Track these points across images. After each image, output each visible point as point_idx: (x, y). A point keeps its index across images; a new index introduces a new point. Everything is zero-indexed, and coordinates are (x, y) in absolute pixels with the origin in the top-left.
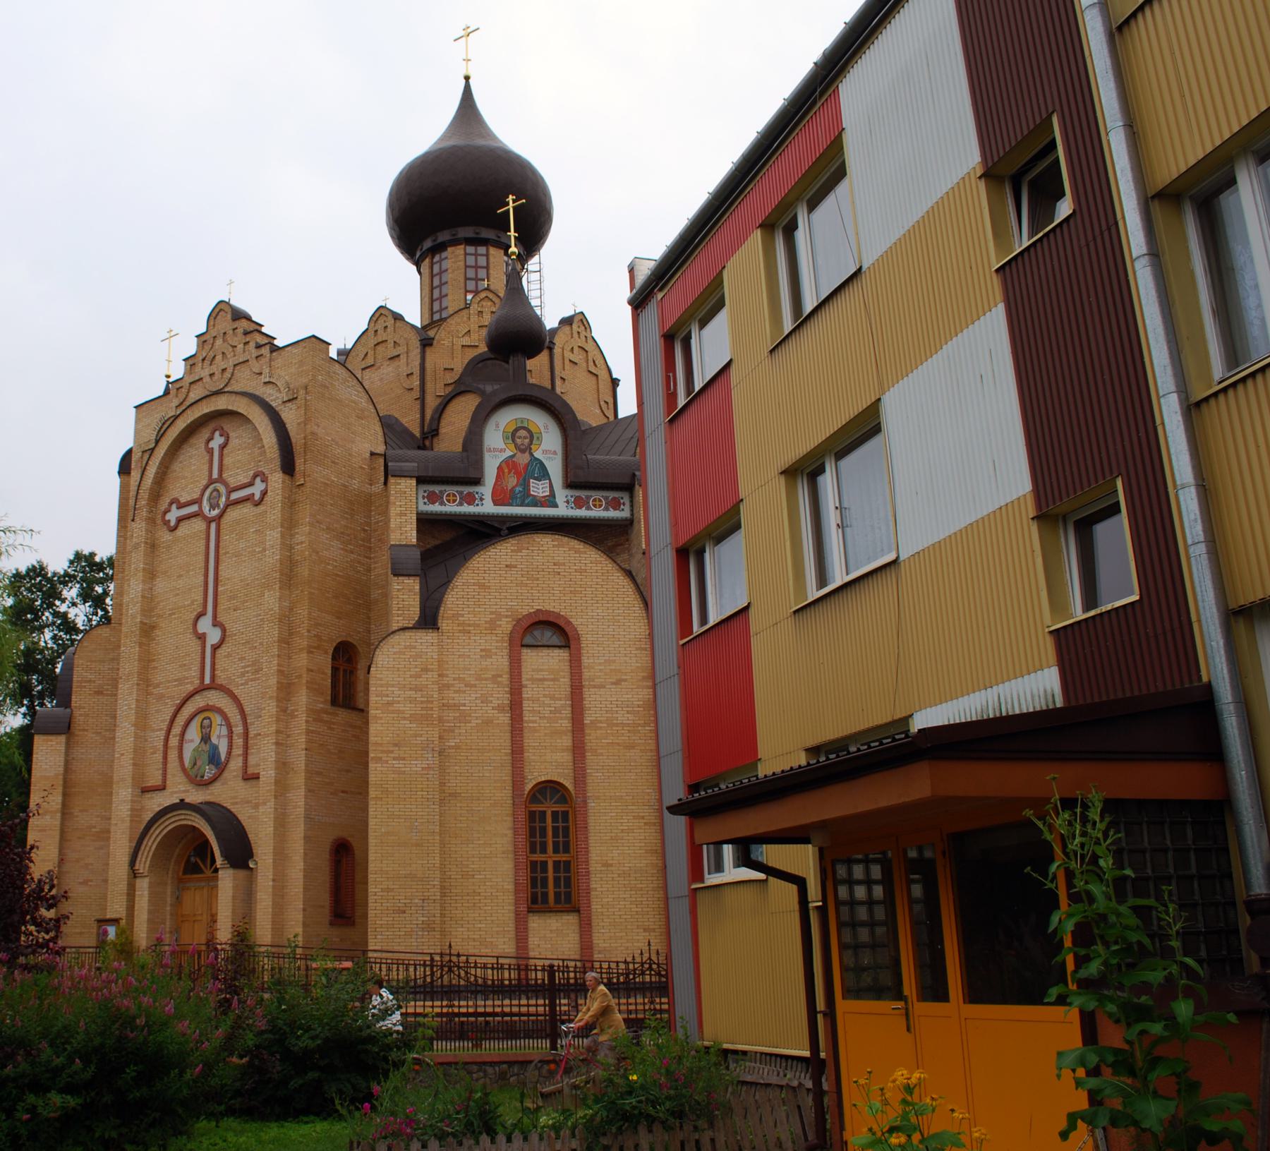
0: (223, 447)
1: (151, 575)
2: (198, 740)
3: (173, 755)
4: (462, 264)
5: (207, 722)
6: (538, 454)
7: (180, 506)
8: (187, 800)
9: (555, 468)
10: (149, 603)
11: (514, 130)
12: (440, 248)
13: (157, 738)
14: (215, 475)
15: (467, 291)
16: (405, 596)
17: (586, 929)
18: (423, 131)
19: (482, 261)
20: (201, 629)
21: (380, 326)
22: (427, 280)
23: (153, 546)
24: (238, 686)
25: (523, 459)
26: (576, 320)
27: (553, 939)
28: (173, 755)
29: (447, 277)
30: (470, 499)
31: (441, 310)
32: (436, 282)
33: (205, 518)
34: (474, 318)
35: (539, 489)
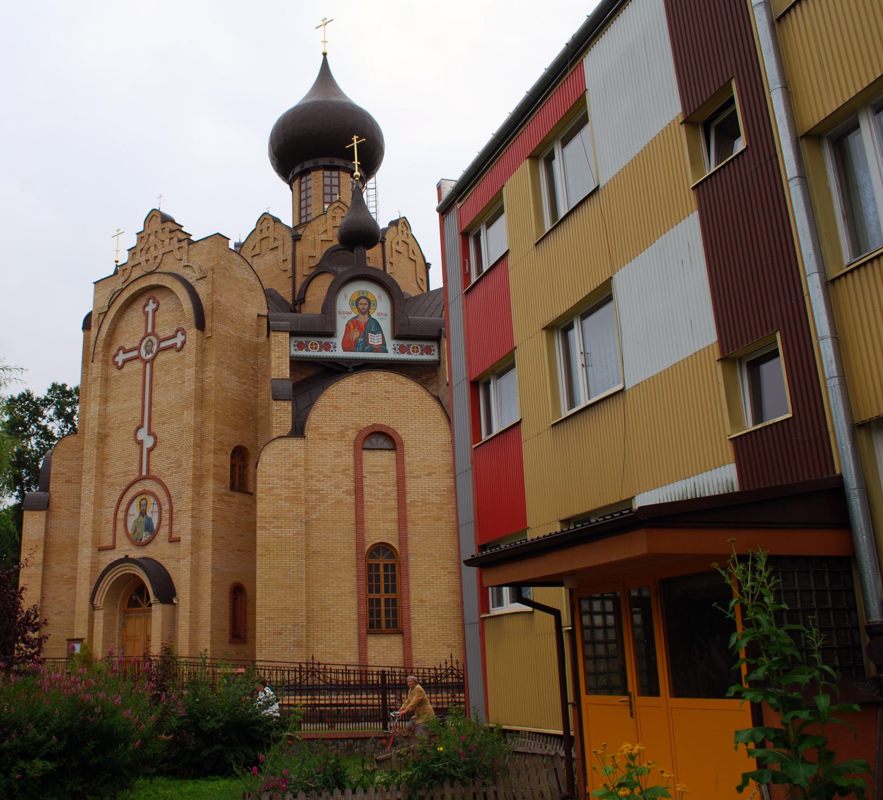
0: (155, 311)
1: (105, 399)
2: (137, 514)
3: (120, 525)
4: (321, 183)
5: (144, 502)
6: (374, 316)
7: (125, 352)
8: (130, 556)
9: (386, 325)
10: (104, 419)
11: (357, 90)
12: (306, 172)
13: (109, 513)
14: (150, 330)
15: (325, 203)
16: (282, 414)
17: (407, 646)
18: (294, 91)
19: (335, 181)
20: (140, 437)
21: (264, 227)
22: (297, 195)
23: (106, 380)
24: (165, 477)
25: (364, 319)
26: (400, 222)
27: (385, 653)
28: (120, 525)
29: (311, 192)
30: (327, 347)
31: (307, 215)
32: (303, 196)
33: (142, 360)
34: (330, 221)
35: (375, 340)
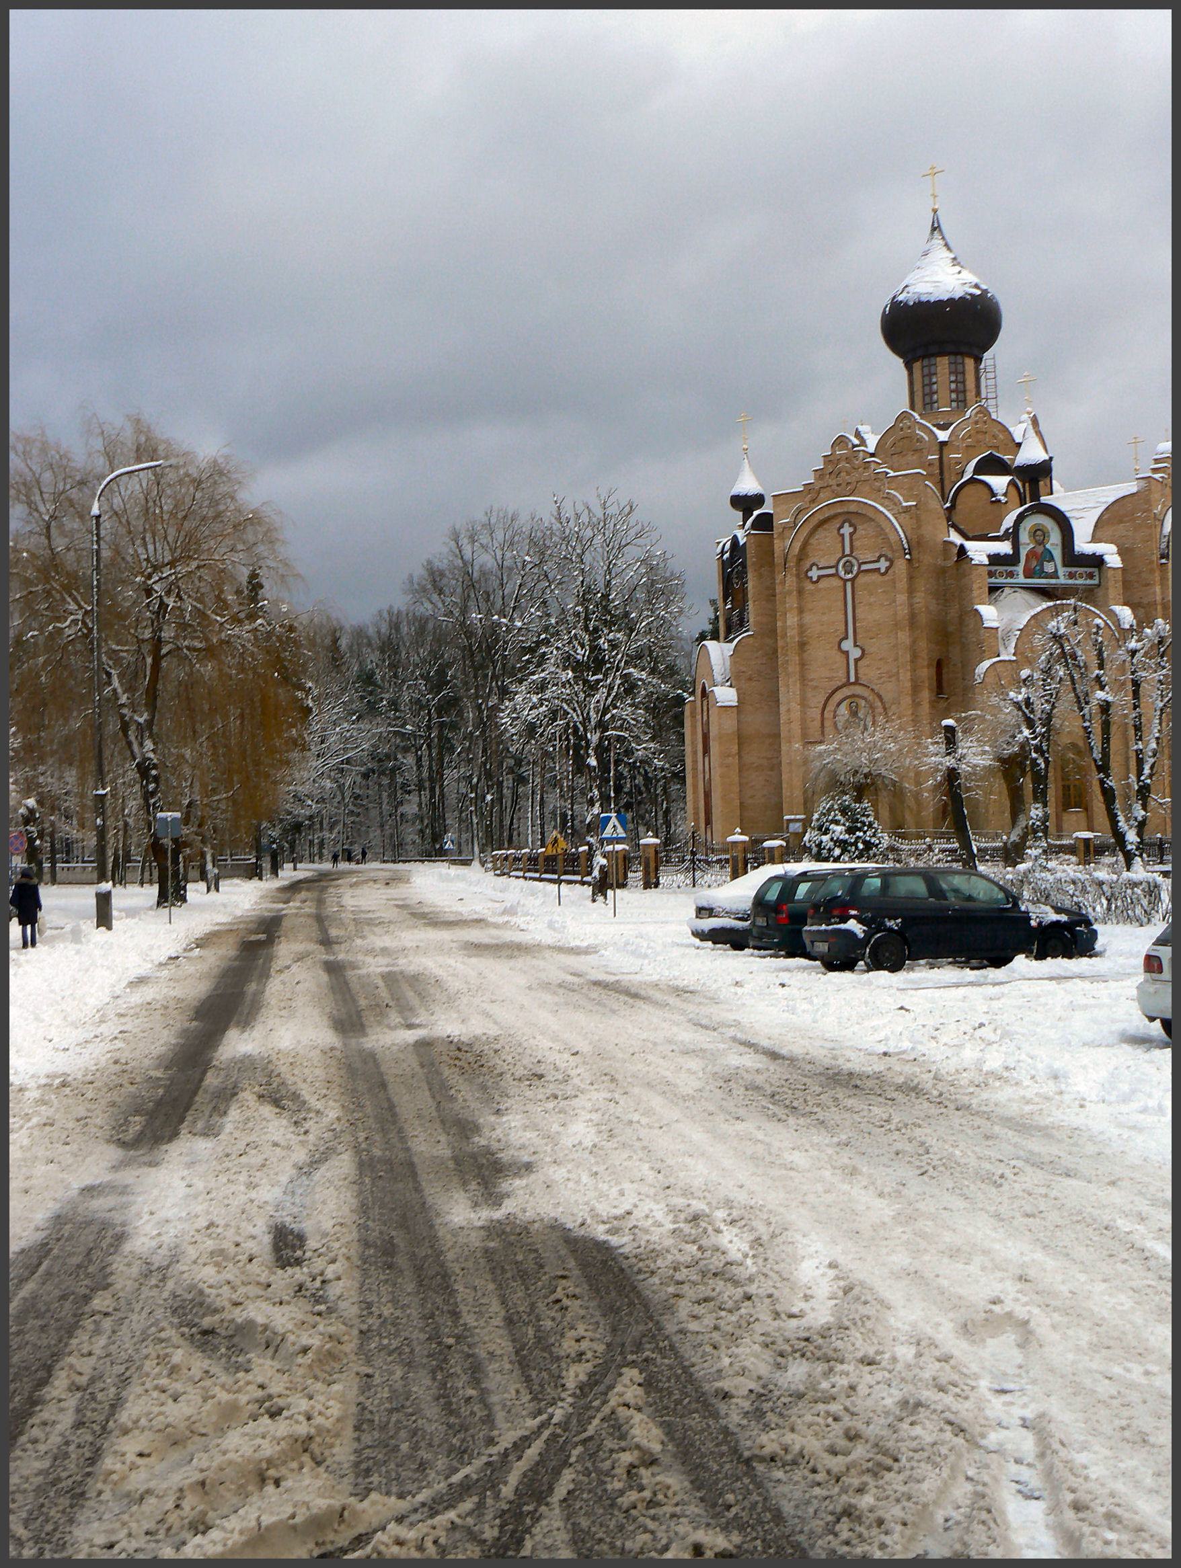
0: (851, 535)
1: (801, 611)
6: (1048, 546)
7: (819, 569)
9: (1057, 554)
10: (802, 628)
13: (815, 713)
14: (847, 551)
23: (800, 592)
25: (1040, 549)
35: (1049, 567)
